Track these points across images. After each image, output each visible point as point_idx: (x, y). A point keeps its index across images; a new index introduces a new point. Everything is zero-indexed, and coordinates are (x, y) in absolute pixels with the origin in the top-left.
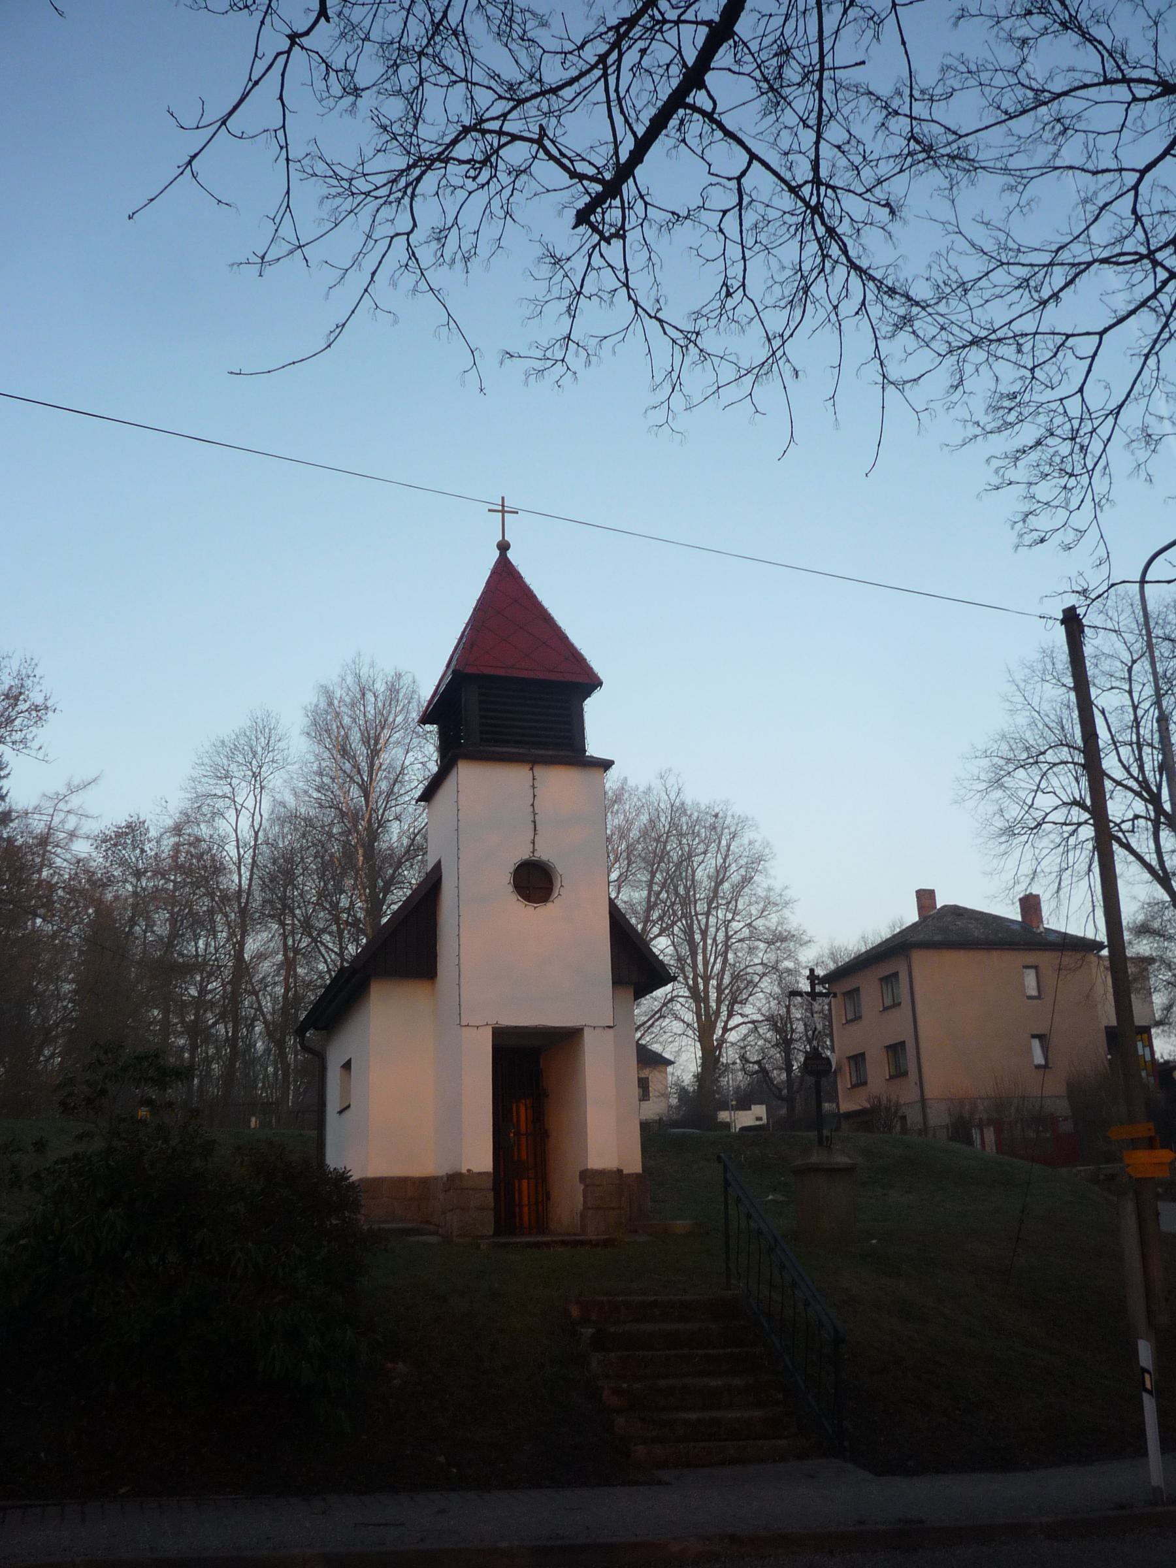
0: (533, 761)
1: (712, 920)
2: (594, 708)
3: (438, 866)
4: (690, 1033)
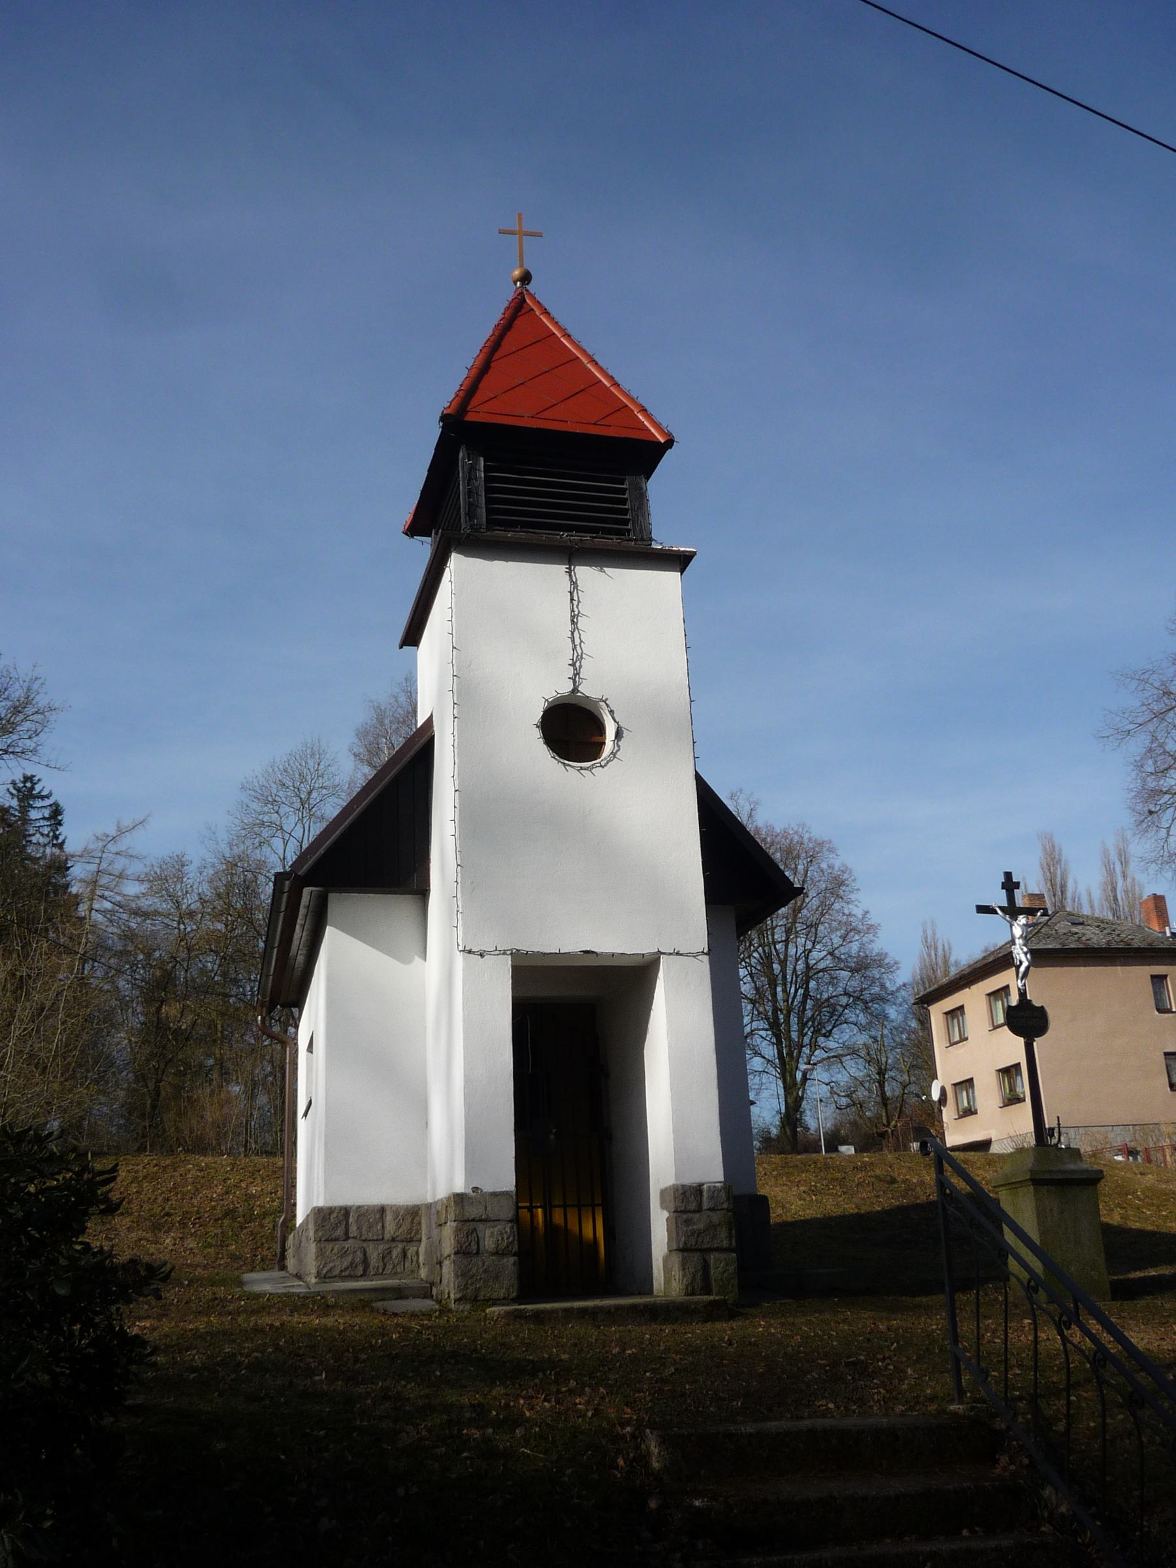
0: (571, 555)
1: (792, 950)
4: (771, 1070)
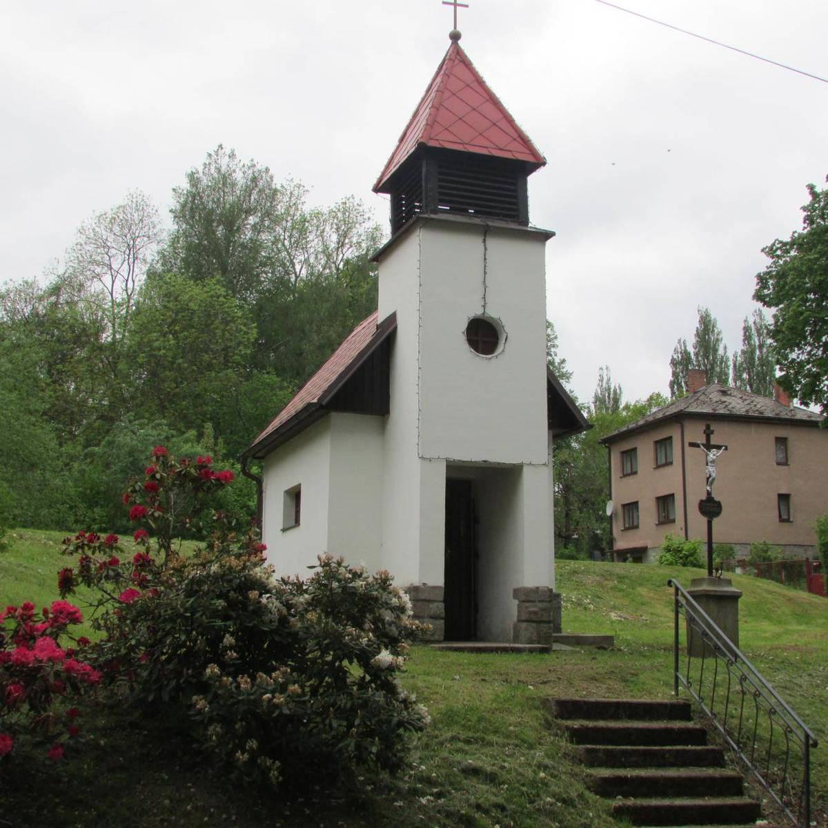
2: (535, 183)
3: (392, 319)
